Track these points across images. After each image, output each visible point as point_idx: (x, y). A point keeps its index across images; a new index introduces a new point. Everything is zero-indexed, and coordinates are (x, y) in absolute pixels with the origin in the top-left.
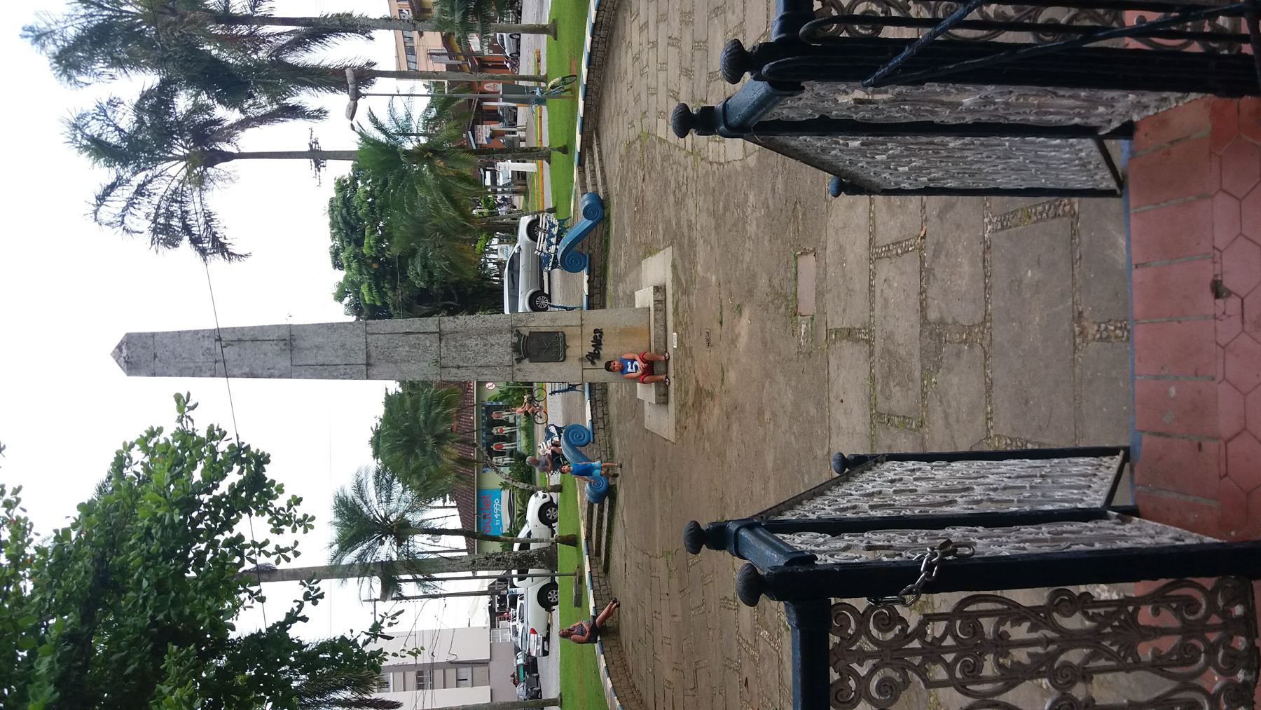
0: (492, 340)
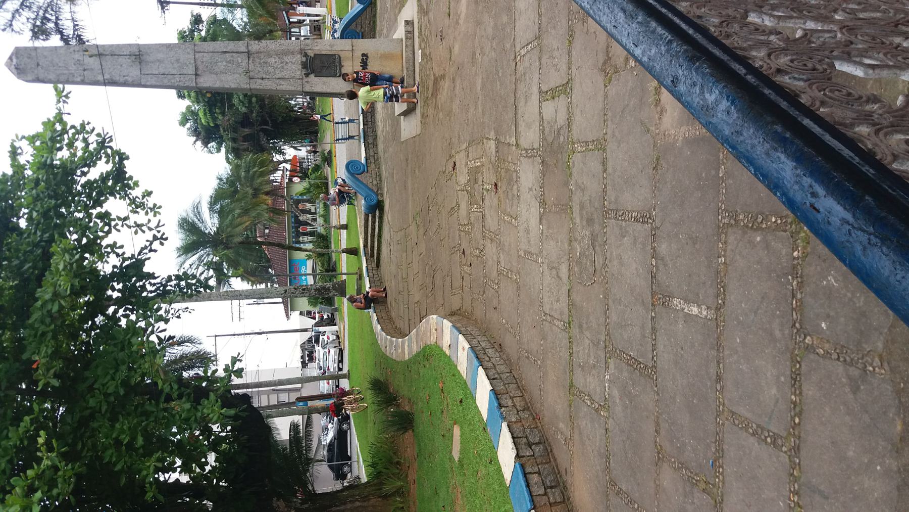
0: (286, 59)
